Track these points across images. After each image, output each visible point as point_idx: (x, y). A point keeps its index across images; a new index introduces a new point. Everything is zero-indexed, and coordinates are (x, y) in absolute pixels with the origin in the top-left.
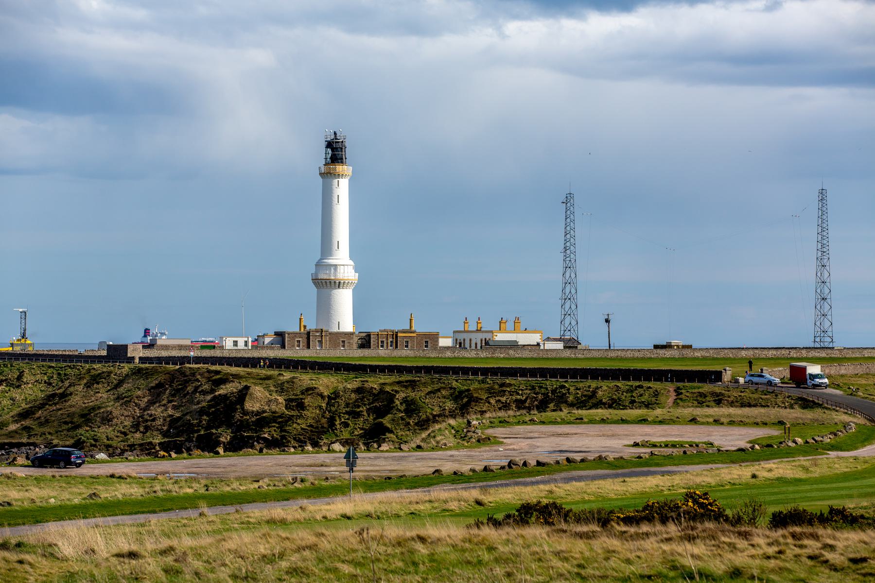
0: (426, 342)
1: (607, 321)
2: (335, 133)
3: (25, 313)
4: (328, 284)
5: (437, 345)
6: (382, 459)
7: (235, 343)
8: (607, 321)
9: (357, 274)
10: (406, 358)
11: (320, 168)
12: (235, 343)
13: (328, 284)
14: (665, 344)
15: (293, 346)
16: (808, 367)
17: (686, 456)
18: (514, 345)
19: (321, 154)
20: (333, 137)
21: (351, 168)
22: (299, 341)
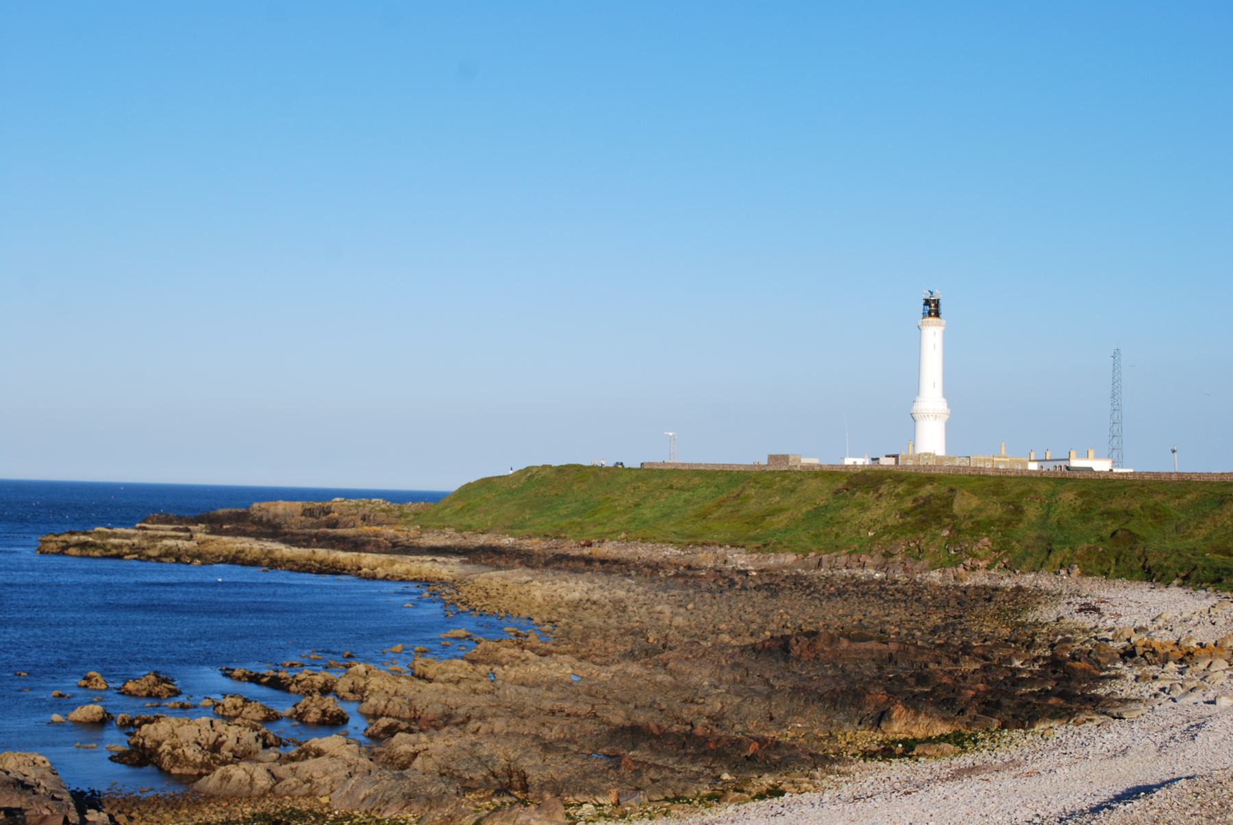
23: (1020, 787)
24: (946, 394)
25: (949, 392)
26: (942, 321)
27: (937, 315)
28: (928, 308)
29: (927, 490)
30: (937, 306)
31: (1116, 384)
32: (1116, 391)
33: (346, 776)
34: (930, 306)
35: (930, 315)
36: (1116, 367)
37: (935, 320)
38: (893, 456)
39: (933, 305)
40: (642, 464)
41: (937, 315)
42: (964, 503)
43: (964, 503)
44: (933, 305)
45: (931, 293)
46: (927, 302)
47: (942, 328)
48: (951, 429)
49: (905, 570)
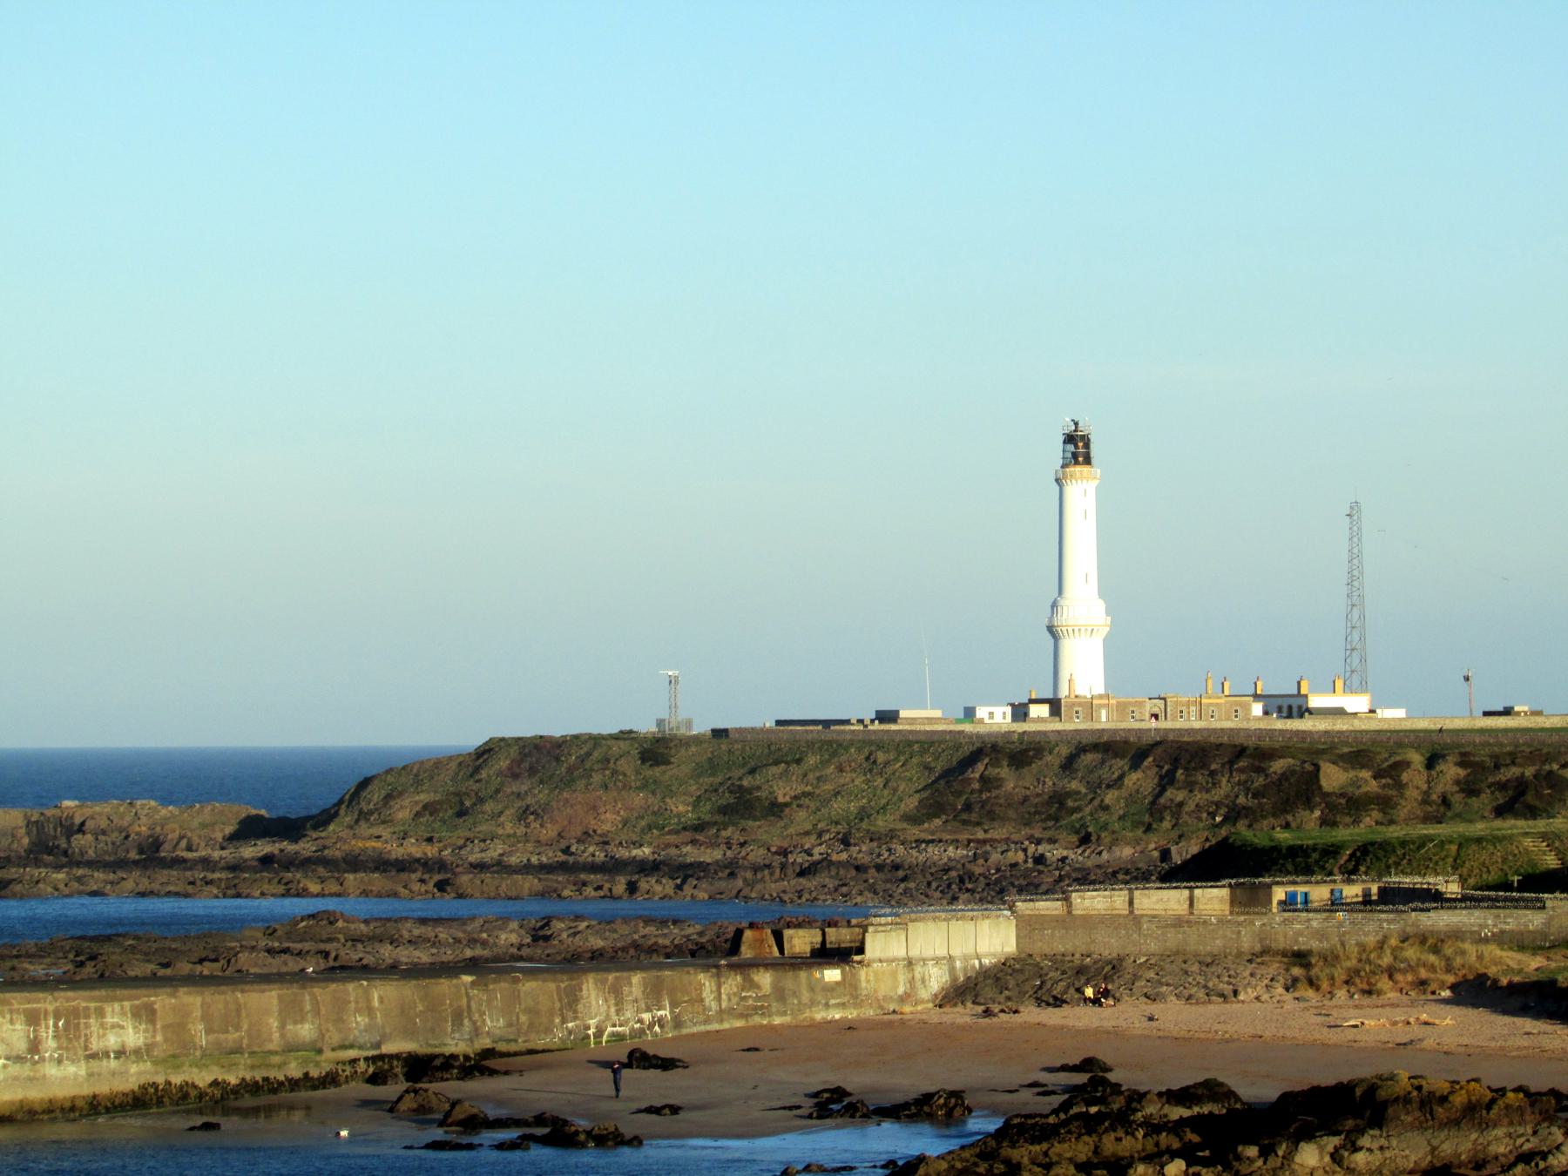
0: (1236, 711)
1: (1467, 679)
2: (1076, 424)
3: (1164, 699)
4: (1089, 632)
5: (1250, 714)
6: (30, 944)
7: (991, 715)
8: (1467, 679)
9: (1109, 618)
10: (930, 720)
11: (1056, 471)
12: (991, 715)
13: (1077, 631)
14: (1502, 709)
15: (1072, 718)
16: (977, 709)
17: (847, 918)
18: (1340, 712)
19: (1056, 450)
20: (1073, 428)
21: (1099, 471)
22: (1077, 712)
23: (364, 806)
24: (1103, 593)
25: (1108, 590)
26: (1095, 471)
27: (1088, 461)
28: (1071, 448)
29: (1278, 766)
30: (1087, 445)
31: (1355, 561)
32: (1355, 573)
33: (136, 1033)
34: (1076, 447)
35: (1077, 463)
36: (1355, 535)
37: (1085, 469)
38: (1160, 698)
39: (1081, 444)
40: (879, 1125)
41: (1088, 461)
42: (1333, 777)
43: (1333, 777)
44: (1081, 444)
45: (1076, 424)
46: (1070, 439)
47: (1096, 482)
48: (1115, 652)
49: (509, 836)
